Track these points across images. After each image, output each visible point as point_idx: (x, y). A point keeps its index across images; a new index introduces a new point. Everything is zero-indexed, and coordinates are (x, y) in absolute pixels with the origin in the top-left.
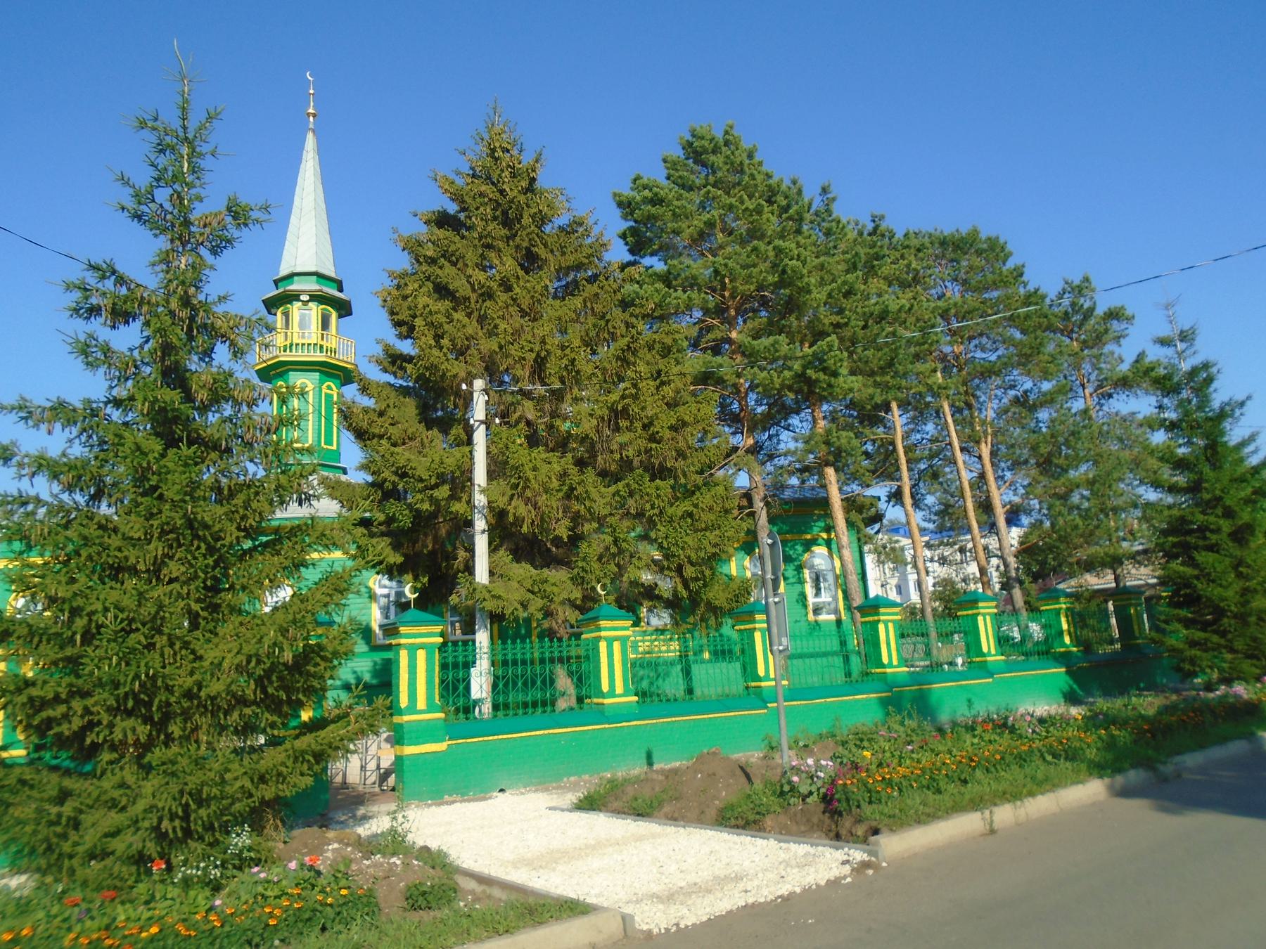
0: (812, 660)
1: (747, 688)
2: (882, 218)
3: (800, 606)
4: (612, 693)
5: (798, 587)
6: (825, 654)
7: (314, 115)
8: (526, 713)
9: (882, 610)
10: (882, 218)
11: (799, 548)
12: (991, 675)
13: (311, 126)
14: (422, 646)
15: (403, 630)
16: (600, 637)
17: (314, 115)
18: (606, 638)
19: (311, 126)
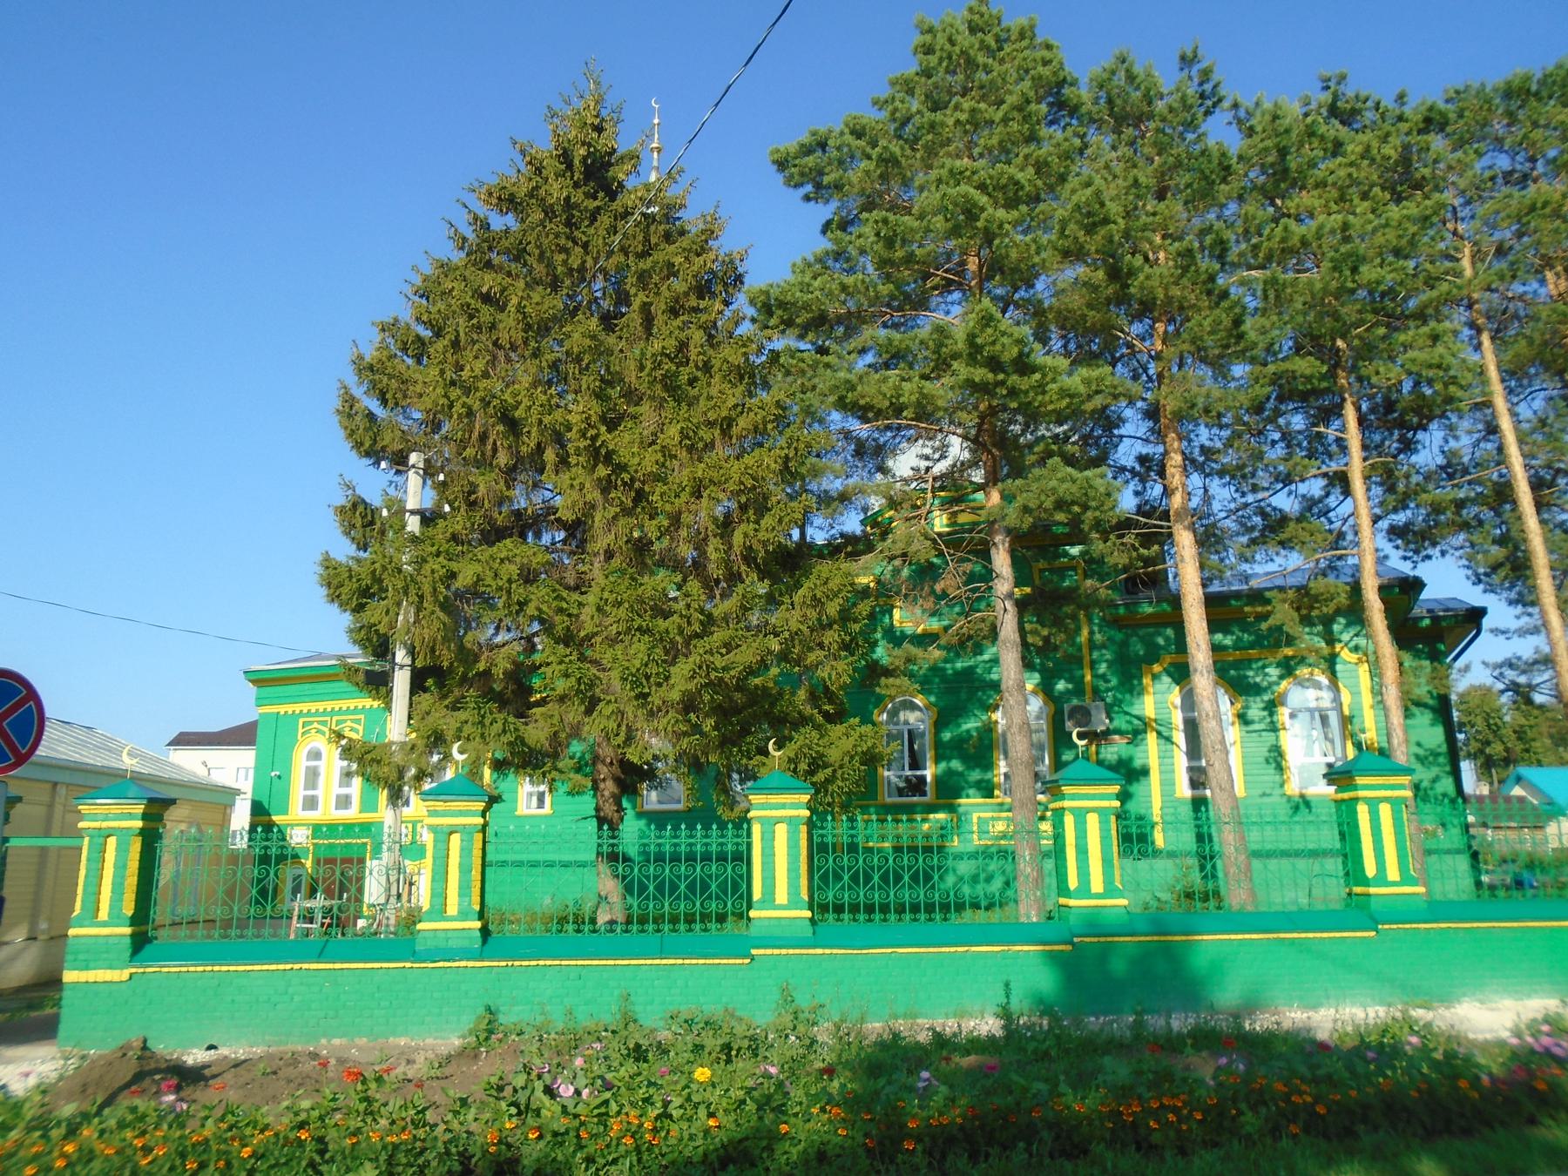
0: (1285, 863)
1: (1349, 894)
2: (1342, 78)
3: (1271, 769)
4: (1381, 878)
5: (1269, 738)
6: (1314, 854)
7: (659, 150)
8: (870, 920)
9: (1360, 781)
10: (1342, 78)
11: (1273, 672)
12: (1373, 922)
13: (655, 164)
14: (779, 820)
15: (1066, 789)
16: (1357, 799)
17: (659, 150)
18: (1367, 800)
19: (655, 164)
